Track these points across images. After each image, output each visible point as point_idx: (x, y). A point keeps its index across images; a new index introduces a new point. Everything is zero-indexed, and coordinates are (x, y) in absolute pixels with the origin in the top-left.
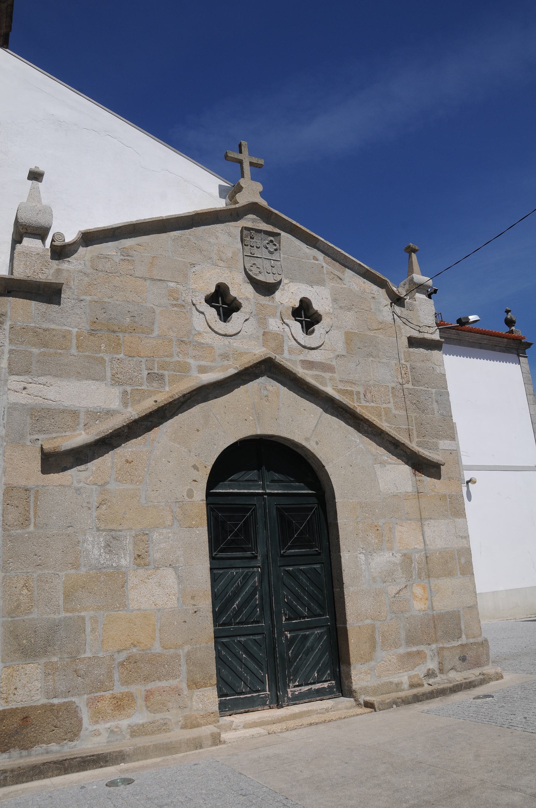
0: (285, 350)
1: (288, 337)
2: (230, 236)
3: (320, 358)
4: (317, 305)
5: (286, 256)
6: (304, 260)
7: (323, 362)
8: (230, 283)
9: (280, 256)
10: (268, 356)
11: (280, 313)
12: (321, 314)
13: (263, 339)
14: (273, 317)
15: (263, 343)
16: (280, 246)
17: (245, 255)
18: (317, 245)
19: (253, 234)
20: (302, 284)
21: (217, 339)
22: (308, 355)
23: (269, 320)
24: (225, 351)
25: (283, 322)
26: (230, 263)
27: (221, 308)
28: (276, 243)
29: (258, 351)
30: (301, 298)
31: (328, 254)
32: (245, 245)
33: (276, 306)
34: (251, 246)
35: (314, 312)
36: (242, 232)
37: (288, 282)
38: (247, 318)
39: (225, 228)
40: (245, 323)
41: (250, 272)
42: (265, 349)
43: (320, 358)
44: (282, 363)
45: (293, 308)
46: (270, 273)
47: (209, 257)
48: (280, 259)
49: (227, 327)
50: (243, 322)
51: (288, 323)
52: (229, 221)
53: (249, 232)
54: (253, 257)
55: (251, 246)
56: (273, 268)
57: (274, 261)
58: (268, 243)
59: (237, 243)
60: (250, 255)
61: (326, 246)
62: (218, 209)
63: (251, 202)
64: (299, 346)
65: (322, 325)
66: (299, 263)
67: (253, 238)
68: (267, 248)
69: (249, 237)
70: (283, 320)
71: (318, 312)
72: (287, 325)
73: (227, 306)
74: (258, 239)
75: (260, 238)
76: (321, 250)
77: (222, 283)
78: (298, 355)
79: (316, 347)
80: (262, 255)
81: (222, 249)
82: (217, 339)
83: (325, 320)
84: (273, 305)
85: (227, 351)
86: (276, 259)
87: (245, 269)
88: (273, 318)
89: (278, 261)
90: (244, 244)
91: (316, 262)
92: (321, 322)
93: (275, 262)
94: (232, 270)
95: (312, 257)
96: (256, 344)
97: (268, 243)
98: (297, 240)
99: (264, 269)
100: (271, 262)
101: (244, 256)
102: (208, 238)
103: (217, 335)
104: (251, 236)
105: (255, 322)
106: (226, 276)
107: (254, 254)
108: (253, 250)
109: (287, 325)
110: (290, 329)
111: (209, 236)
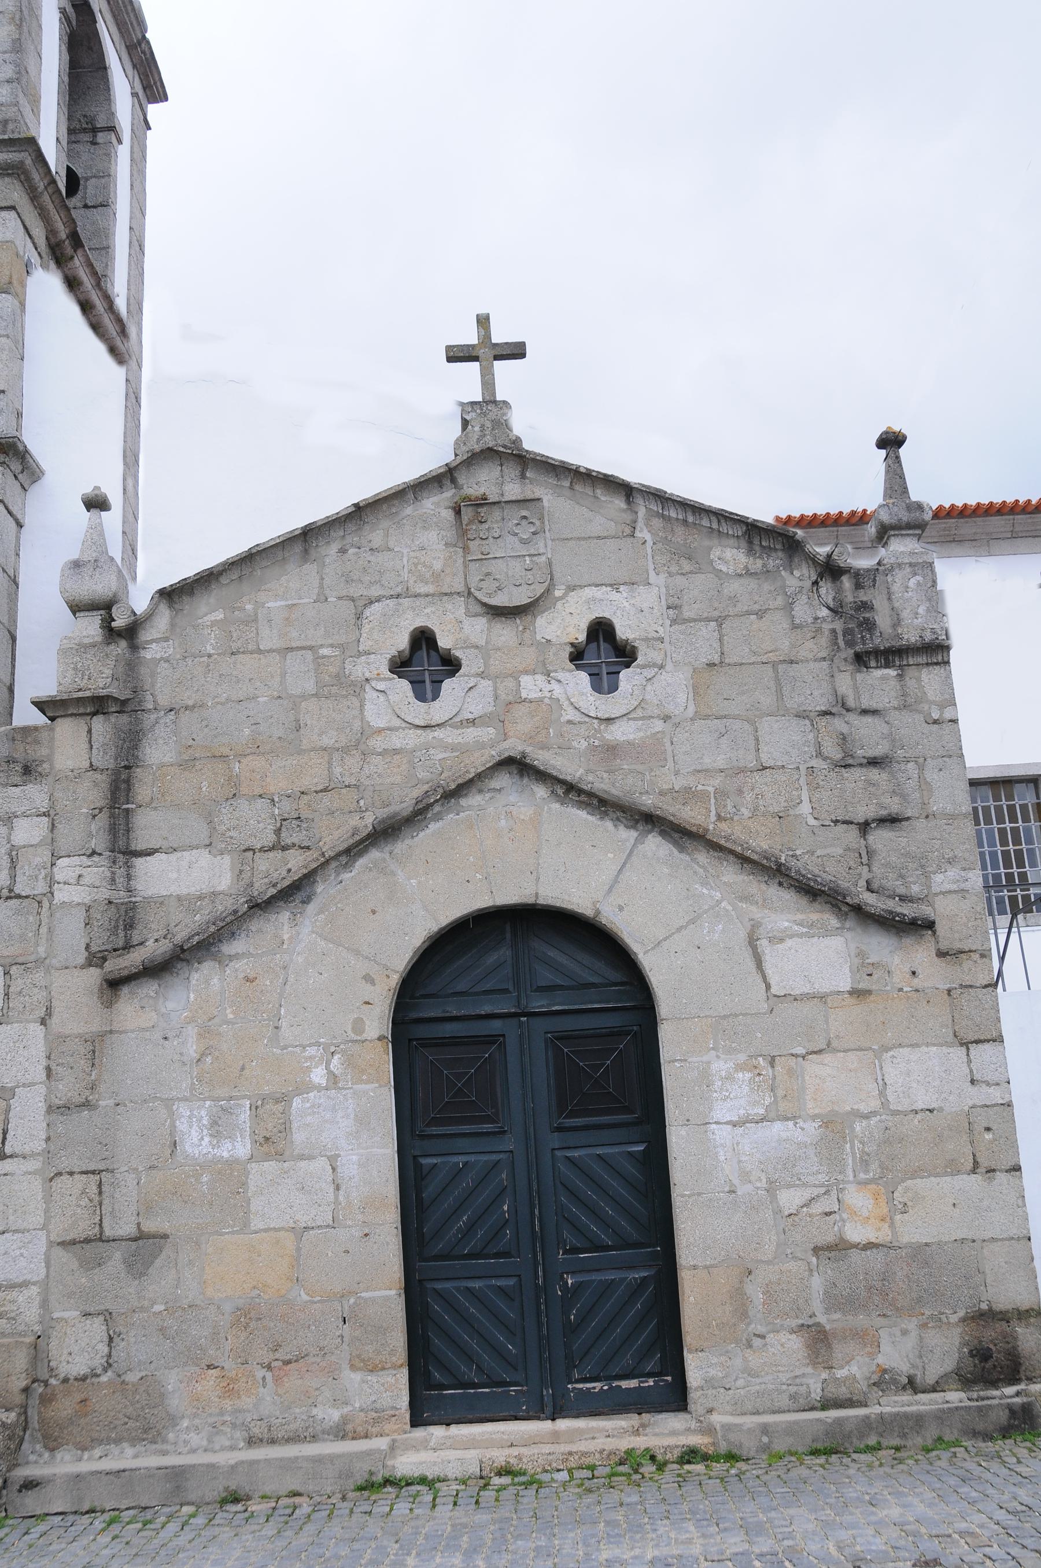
60: (480, 557)
108: (487, 547)
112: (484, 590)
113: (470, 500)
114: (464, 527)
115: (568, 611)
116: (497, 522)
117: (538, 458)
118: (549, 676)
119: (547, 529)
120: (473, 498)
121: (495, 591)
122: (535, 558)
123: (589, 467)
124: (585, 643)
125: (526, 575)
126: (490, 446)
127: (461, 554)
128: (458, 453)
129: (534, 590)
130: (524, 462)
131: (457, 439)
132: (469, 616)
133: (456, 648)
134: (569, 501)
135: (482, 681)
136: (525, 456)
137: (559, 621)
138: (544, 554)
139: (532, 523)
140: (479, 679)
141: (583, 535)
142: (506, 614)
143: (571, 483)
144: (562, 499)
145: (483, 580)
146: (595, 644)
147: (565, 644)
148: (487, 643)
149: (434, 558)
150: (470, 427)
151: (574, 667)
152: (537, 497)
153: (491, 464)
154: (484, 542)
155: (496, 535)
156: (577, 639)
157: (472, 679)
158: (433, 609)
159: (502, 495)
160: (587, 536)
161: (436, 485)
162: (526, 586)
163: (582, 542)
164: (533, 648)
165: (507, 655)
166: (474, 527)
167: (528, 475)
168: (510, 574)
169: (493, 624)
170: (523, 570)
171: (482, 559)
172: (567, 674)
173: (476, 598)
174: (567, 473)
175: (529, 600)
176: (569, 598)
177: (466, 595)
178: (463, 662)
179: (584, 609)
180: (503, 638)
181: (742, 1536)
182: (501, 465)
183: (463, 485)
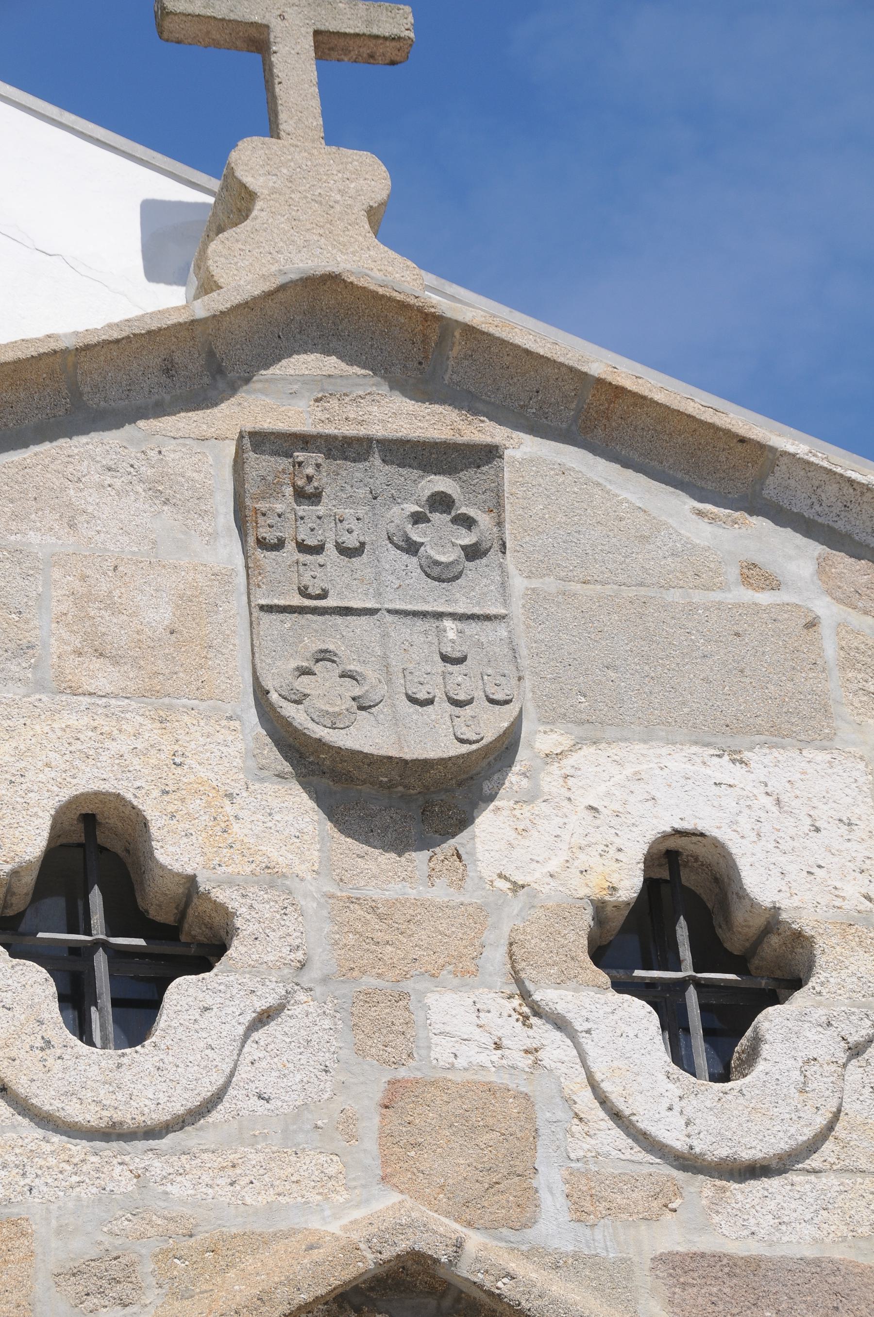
0: (544, 1196)
1: (569, 1101)
2: (166, 502)
3: (808, 1231)
4: (776, 872)
5: (550, 584)
6: (674, 596)
7: (837, 1256)
8: (156, 793)
9: (503, 585)
10: (403, 1246)
11: (504, 949)
12: (808, 931)
13: (386, 1136)
14: (456, 982)
15: (385, 1163)
16: (500, 524)
17: (262, 608)
18: (770, 491)
19: (310, 471)
20: (664, 751)
21: (52, 1161)
22: (716, 1219)
23: (431, 999)
24: (107, 1240)
25: (526, 1010)
26: (161, 665)
27: (692, 996)
28: (472, 512)
29: (345, 1221)
30: (651, 835)
31: (849, 536)
32: (262, 544)
33: (480, 908)
34: (302, 548)
35: (758, 922)
36: (239, 465)
37: (567, 742)
38: (272, 1001)
39: (133, 450)
40: (255, 1036)
41: (289, 710)
42: (395, 1197)
43: (808, 1231)
44: (504, 1286)
45: (600, 909)
46: (430, 702)
47: (12, 646)
48: (505, 604)
49: (126, 1076)
50: (241, 1030)
51: (561, 1008)
52: (159, 410)
53: (284, 463)
54: (314, 611)
55: (302, 548)
56: (450, 668)
57: (460, 625)
58: (418, 519)
59: (214, 536)
60: (297, 600)
61: (832, 489)
62: (70, 343)
63: (294, 276)
64: (650, 1158)
65: (819, 1004)
66: (641, 616)
67: (315, 498)
68: (411, 548)
69: (289, 491)
70: (525, 995)
71: (784, 916)
72: (560, 1024)
73: (141, 942)
74: (351, 501)
75: (362, 492)
76: (800, 516)
77: (97, 794)
78: (643, 1227)
79: (780, 1157)
80: (378, 594)
81: (104, 586)
82: (52, 1161)
83: (840, 966)
84: (459, 899)
85: (118, 1242)
86: (477, 610)
87: (261, 694)
88: (455, 990)
89: (488, 618)
90: (251, 540)
91: (764, 598)
92: (813, 982)
93: (472, 628)
94: (170, 707)
95: (733, 573)
96: (332, 1170)
97: (418, 519)
98: (630, 473)
99: (389, 682)
100: (441, 632)
101: (256, 613)
102: (13, 526)
103: (56, 1139)
104: (300, 483)
105: (327, 1023)
106: (124, 749)
107: (324, 595)
108: (319, 572)
109: (560, 1024)
110: (577, 1046)
111: (15, 516)
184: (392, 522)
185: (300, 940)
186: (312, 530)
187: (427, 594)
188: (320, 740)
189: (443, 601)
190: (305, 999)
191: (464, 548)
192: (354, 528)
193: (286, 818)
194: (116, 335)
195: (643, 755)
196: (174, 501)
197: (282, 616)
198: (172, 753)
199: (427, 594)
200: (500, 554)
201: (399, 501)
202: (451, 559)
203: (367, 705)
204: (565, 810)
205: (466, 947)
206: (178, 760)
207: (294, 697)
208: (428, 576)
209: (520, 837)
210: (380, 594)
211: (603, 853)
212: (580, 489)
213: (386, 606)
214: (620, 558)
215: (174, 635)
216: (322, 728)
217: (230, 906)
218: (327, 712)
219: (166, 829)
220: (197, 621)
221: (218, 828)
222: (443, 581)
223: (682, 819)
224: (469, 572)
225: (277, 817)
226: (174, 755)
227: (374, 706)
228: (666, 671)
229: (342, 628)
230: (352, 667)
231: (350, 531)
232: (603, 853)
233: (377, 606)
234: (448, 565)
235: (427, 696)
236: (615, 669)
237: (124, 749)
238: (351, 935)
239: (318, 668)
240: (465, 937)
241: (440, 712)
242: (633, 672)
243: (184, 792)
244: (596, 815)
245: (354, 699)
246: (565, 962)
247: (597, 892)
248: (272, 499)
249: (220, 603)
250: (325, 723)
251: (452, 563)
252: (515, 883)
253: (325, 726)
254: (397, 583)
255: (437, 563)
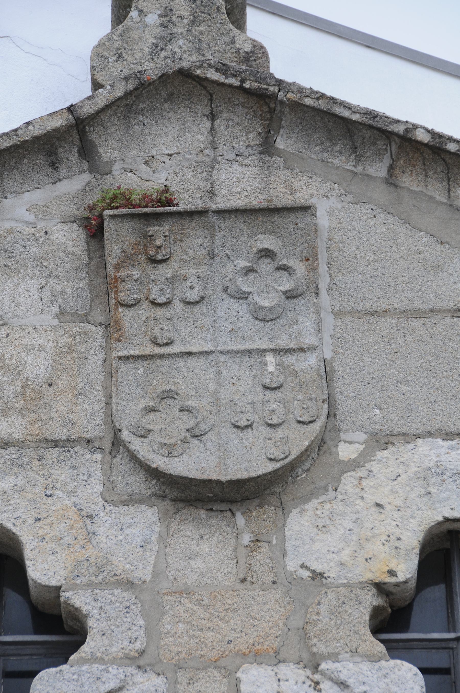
8: (31, 521)
54: (162, 356)
60: (149, 349)
108: (167, 325)
112: (156, 437)
113: (129, 204)
114: (111, 271)
115: (371, 498)
116: (195, 262)
117: (308, 101)
118: (316, 668)
119: (323, 285)
120: (135, 198)
121: (184, 441)
122: (290, 360)
123: (439, 129)
124: (413, 584)
125: (265, 402)
126: (185, 64)
127: (100, 340)
128: (100, 79)
129: (285, 440)
130: (272, 111)
131: (100, 45)
132: (113, 503)
133: (75, 587)
134: (383, 216)
135: (140, 677)
136: (274, 97)
137: (348, 524)
138: (313, 348)
139: (284, 268)
140: (131, 670)
141: (417, 304)
142: (210, 500)
143: (391, 168)
144: (365, 208)
145: (153, 410)
146: (443, 586)
147: (362, 585)
148: (156, 574)
149: (29, 349)
150: (134, 14)
151: (381, 648)
152: (301, 202)
153: (185, 113)
154: (160, 312)
155: (193, 296)
156: (392, 573)
157: (113, 670)
158: (20, 481)
159: (212, 193)
160: (427, 307)
161: (40, 159)
162: (265, 431)
163: (414, 323)
164: (278, 594)
165: (208, 607)
166: (136, 274)
167: (280, 144)
168: (224, 395)
169: (174, 526)
170: (259, 389)
171: (151, 357)
172: (365, 666)
173: (133, 457)
174: (381, 144)
175: (272, 467)
176: (374, 466)
177: (107, 446)
178: (91, 623)
179: (413, 495)
180: (198, 564)
181: (164, 254)
182: (213, 117)
183: (111, 164)
184: (226, 277)
185: (138, 633)
186: (162, 290)
187: (255, 334)
188: (157, 469)
189: (266, 339)
190: (141, 680)
191: (284, 293)
192: (195, 285)
193: (134, 531)
194: (36, 131)
195: (425, 456)
196: (57, 273)
197: (136, 364)
198: (45, 486)
199: (255, 334)
200: (314, 295)
201: (233, 258)
202: (273, 304)
203: (199, 434)
204: (358, 507)
205: (271, 628)
206: (48, 493)
207: (139, 433)
208: (256, 319)
209: (320, 533)
210: (215, 339)
211: (385, 542)
212: (388, 229)
213: (220, 348)
214: (418, 287)
215: (52, 387)
216: (160, 457)
217: (84, 610)
218: (165, 444)
219: (37, 550)
220: (70, 373)
221: (78, 546)
222: (268, 321)
223: (452, 509)
224: (289, 313)
225: (127, 531)
226: (46, 488)
227: (205, 434)
228: (449, 382)
229: (184, 369)
230: (189, 403)
231: (192, 288)
232: (385, 542)
233: (213, 349)
234: (270, 309)
235: (246, 423)
236: (408, 383)
237: (7, 486)
238: (180, 625)
239: (163, 406)
240: (272, 619)
241: (257, 435)
242: (421, 385)
243: (52, 518)
244: (381, 510)
245: (188, 430)
246: (350, 636)
247: (378, 575)
248: (130, 267)
249: (89, 357)
250: (163, 453)
251: (274, 307)
252: (313, 571)
253: (163, 456)
254: (230, 327)
255: (263, 308)
